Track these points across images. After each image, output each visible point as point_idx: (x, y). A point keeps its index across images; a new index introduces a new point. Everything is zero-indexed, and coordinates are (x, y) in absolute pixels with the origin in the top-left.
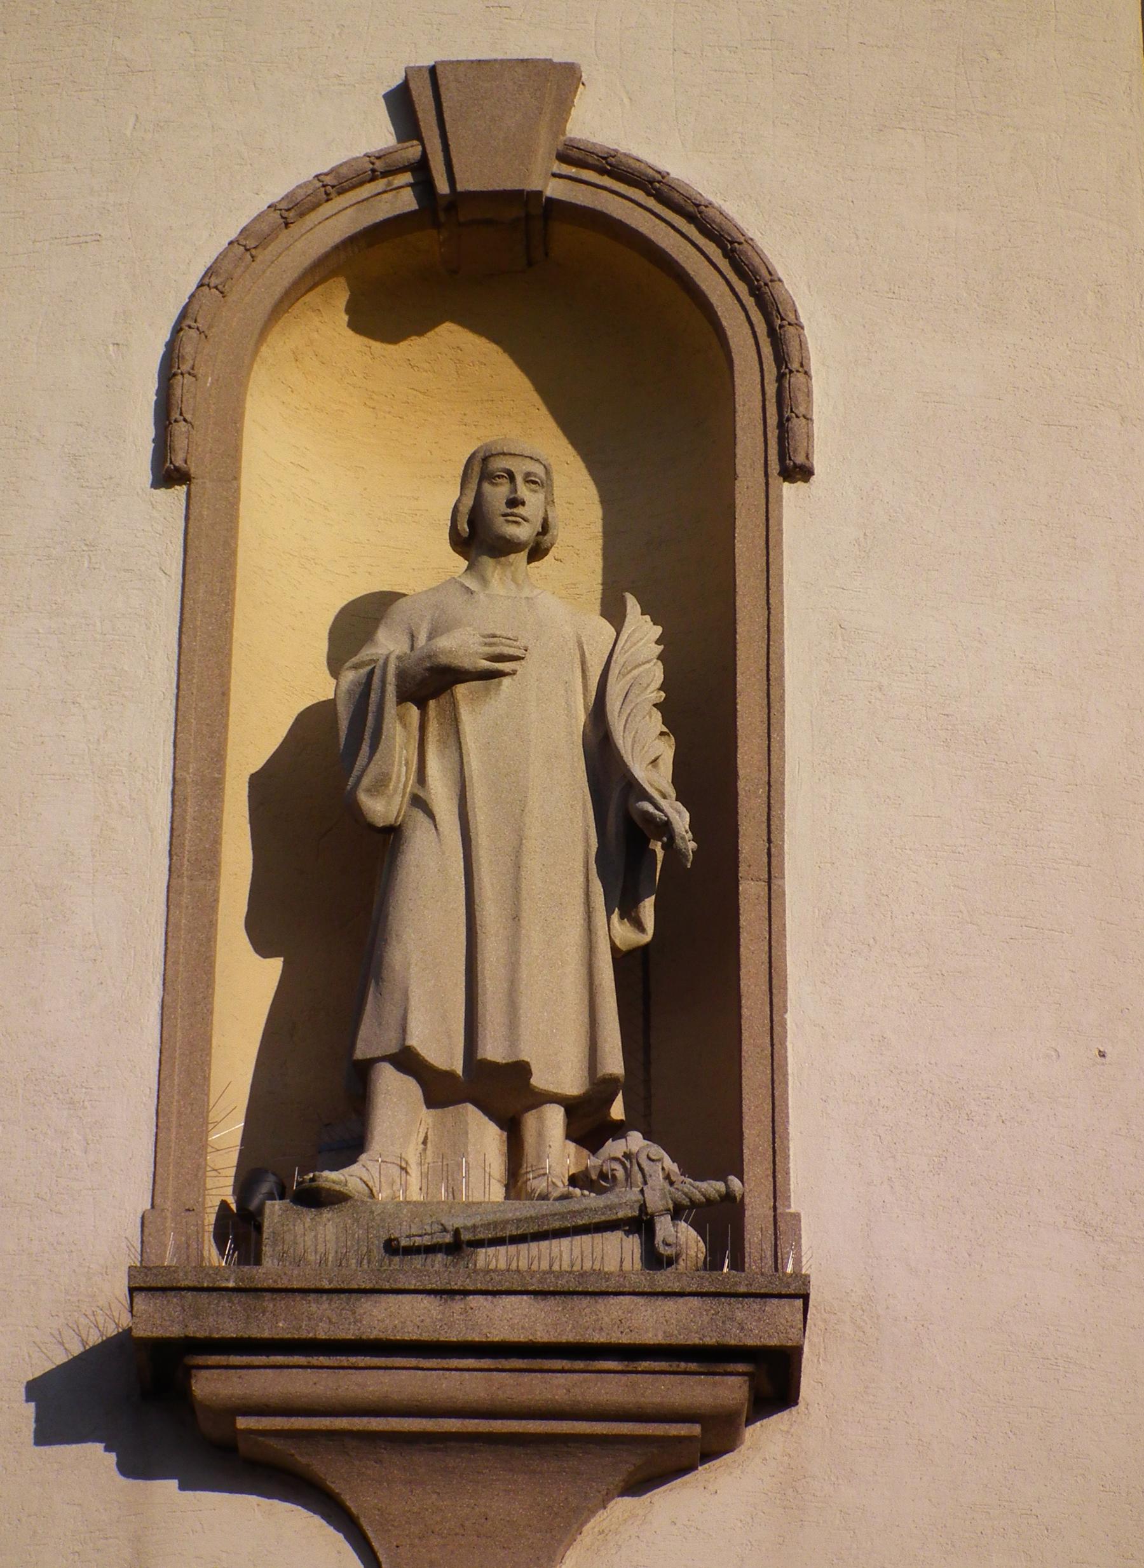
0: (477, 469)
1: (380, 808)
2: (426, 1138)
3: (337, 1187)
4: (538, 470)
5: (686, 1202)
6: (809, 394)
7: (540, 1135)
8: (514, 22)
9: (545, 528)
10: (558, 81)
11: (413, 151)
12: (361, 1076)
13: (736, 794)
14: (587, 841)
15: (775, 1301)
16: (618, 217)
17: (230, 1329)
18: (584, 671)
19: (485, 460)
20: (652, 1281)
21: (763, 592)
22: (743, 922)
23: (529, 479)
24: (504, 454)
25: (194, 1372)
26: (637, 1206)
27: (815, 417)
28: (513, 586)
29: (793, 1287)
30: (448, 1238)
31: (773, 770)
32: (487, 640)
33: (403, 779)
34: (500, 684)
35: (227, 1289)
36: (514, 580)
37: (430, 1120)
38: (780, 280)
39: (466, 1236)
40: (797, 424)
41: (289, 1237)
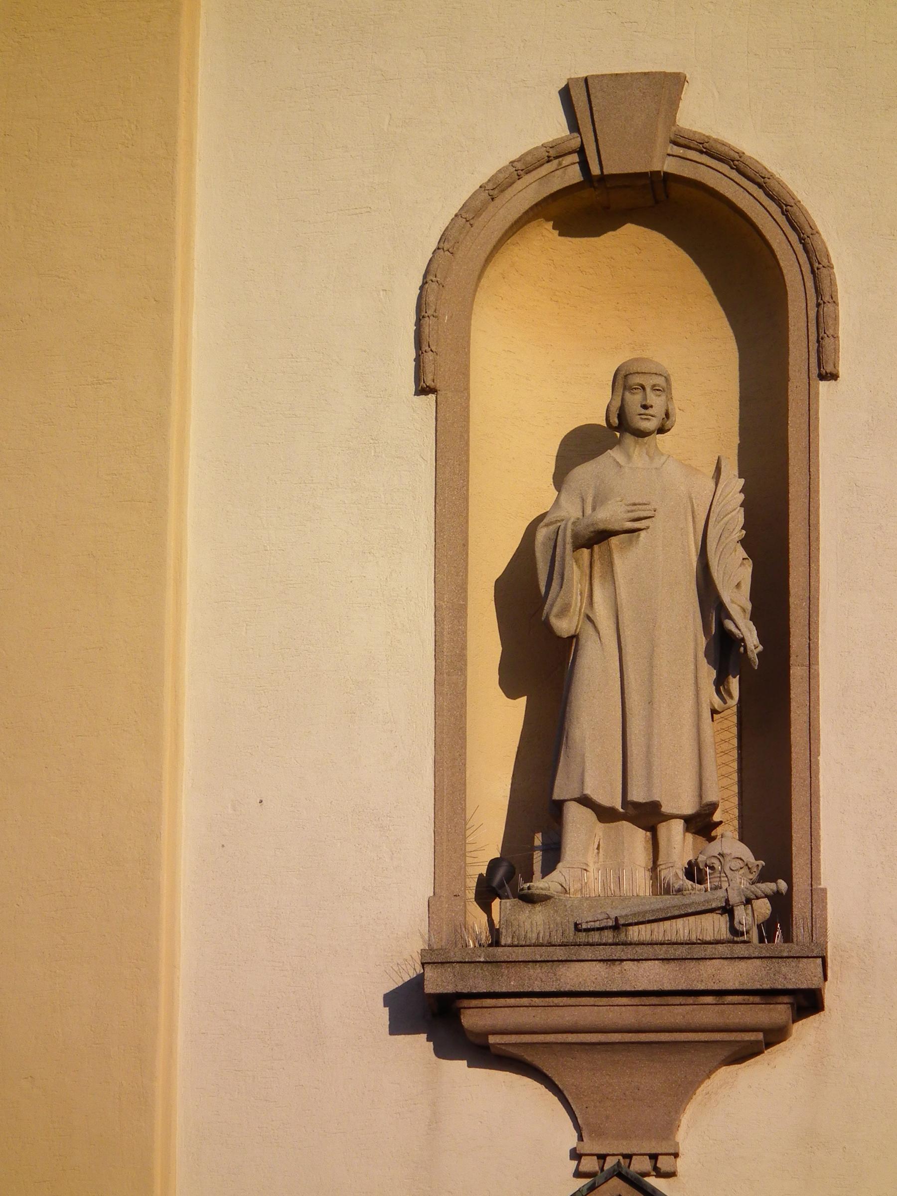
0: (620, 381)
1: (563, 626)
2: (599, 845)
3: (544, 892)
4: (660, 381)
5: (753, 897)
6: (836, 318)
7: (669, 840)
8: (641, 35)
9: (667, 415)
10: (668, 86)
11: (575, 143)
12: (558, 807)
13: (788, 607)
14: (696, 640)
15: (805, 960)
16: (712, 186)
17: (483, 987)
18: (694, 522)
19: (626, 376)
20: (732, 952)
21: (806, 462)
22: (792, 696)
23: (654, 388)
24: (638, 373)
25: (462, 1010)
26: (723, 900)
27: (840, 335)
28: (647, 458)
29: (815, 952)
30: (611, 923)
31: (812, 589)
32: (629, 508)
33: (579, 604)
34: (639, 536)
35: (479, 962)
36: (647, 453)
37: (601, 834)
38: (817, 232)
39: (621, 921)
40: (827, 342)
41: (515, 923)
